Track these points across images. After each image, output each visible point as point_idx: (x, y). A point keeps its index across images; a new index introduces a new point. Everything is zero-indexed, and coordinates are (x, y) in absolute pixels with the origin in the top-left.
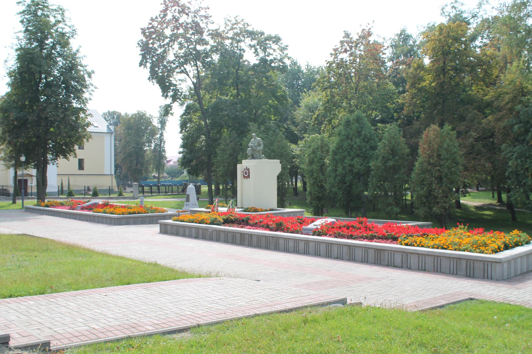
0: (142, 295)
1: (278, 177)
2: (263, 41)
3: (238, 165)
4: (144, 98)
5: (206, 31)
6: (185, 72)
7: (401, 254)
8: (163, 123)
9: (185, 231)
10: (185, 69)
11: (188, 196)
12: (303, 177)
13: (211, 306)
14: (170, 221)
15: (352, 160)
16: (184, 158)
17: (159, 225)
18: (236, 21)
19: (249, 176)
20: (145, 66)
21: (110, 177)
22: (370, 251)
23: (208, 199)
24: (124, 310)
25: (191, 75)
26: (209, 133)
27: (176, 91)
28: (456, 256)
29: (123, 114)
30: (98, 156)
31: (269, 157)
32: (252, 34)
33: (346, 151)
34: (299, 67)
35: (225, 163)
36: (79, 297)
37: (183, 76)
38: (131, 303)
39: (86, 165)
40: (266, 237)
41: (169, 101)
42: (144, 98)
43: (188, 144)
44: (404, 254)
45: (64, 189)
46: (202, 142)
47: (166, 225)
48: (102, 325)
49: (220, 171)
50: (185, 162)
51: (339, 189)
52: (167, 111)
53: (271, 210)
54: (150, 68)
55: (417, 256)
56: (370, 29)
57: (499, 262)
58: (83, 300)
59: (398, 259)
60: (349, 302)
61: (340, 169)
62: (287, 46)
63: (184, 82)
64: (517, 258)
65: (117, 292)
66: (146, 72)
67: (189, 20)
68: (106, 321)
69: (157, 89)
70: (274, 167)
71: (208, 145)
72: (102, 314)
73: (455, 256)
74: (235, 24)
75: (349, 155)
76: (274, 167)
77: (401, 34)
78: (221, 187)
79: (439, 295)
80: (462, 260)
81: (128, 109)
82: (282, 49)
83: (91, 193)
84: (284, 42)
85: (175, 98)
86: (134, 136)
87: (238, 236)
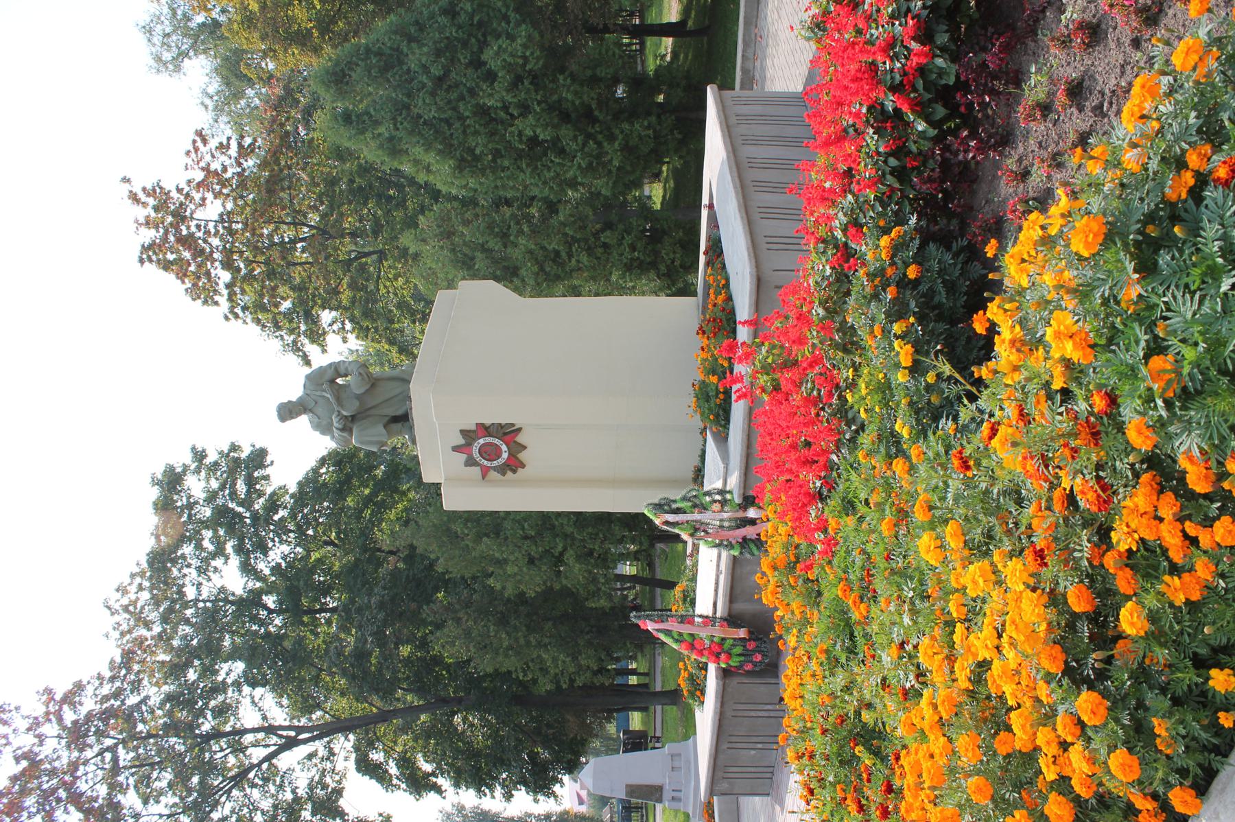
3: (447, 506)
15: (491, 77)
19: (508, 433)
23: (659, 708)
26: (445, 701)
33: (455, 109)
35: (528, 643)
46: (472, 725)
49: (555, 660)
51: (611, 138)
62: (193, 448)
71: (479, 706)
75: (472, 92)
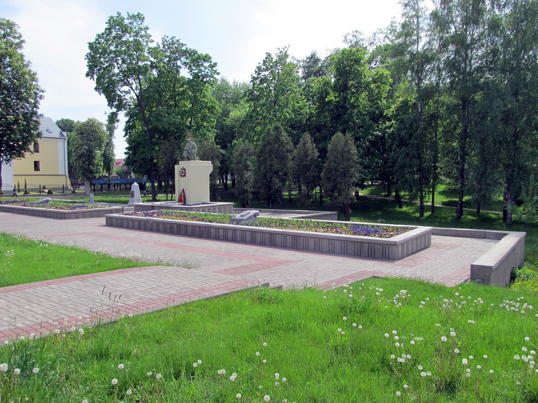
0: (77, 288)
1: (211, 175)
2: (196, 59)
4: (88, 105)
5: (147, 49)
6: (128, 84)
7: (314, 239)
8: (111, 129)
9: (128, 224)
10: (129, 82)
11: (133, 192)
12: (232, 175)
13: (143, 296)
14: (116, 215)
16: (128, 158)
17: (105, 218)
18: (173, 41)
19: (185, 175)
20: (92, 77)
21: (64, 178)
22: (288, 237)
24: (56, 304)
25: (134, 87)
27: (121, 101)
28: (360, 241)
29: (76, 121)
30: (52, 157)
31: (202, 159)
32: (185, 53)
34: (227, 84)
36: (12, 293)
37: (126, 88)
38: (65, 297)
39: (41, 166)
40: (200, 227)
41: (114, 110)
42: (88, 105)
43: (134, 147)
44: (316, 240)
45: (20, 188)
47: (111, 218)
48: (28, 323)
50: (129, 162)
52: (113, 118)
53: (203, 204)
54: (97, 79)
55: (328, 240)
56: (286, 52)
57: (395, 244)
58: (15, 296)
59: (312, 243)
60: (271, 285)
61: (262, 168)
63: (130, 93)
64: (409, 241)
65: (52, 286)
66: (93, 83)
67: (131, 39)
68: (33, 318)
69: (103, 99)
70: (208, 166)
72: (31, 311)
73: (359, 240)
74: (172, 44)
76: (208, 166)
77: (311, 58)
78: (163, 184)
79: (347, 274)
80: (365, 244)
81: (79, 117)
82: (212, 66)
83: (47, 191)
84: (214, 61)
85: (120, 107)
86: (84, 141)
87: (175, 226)
